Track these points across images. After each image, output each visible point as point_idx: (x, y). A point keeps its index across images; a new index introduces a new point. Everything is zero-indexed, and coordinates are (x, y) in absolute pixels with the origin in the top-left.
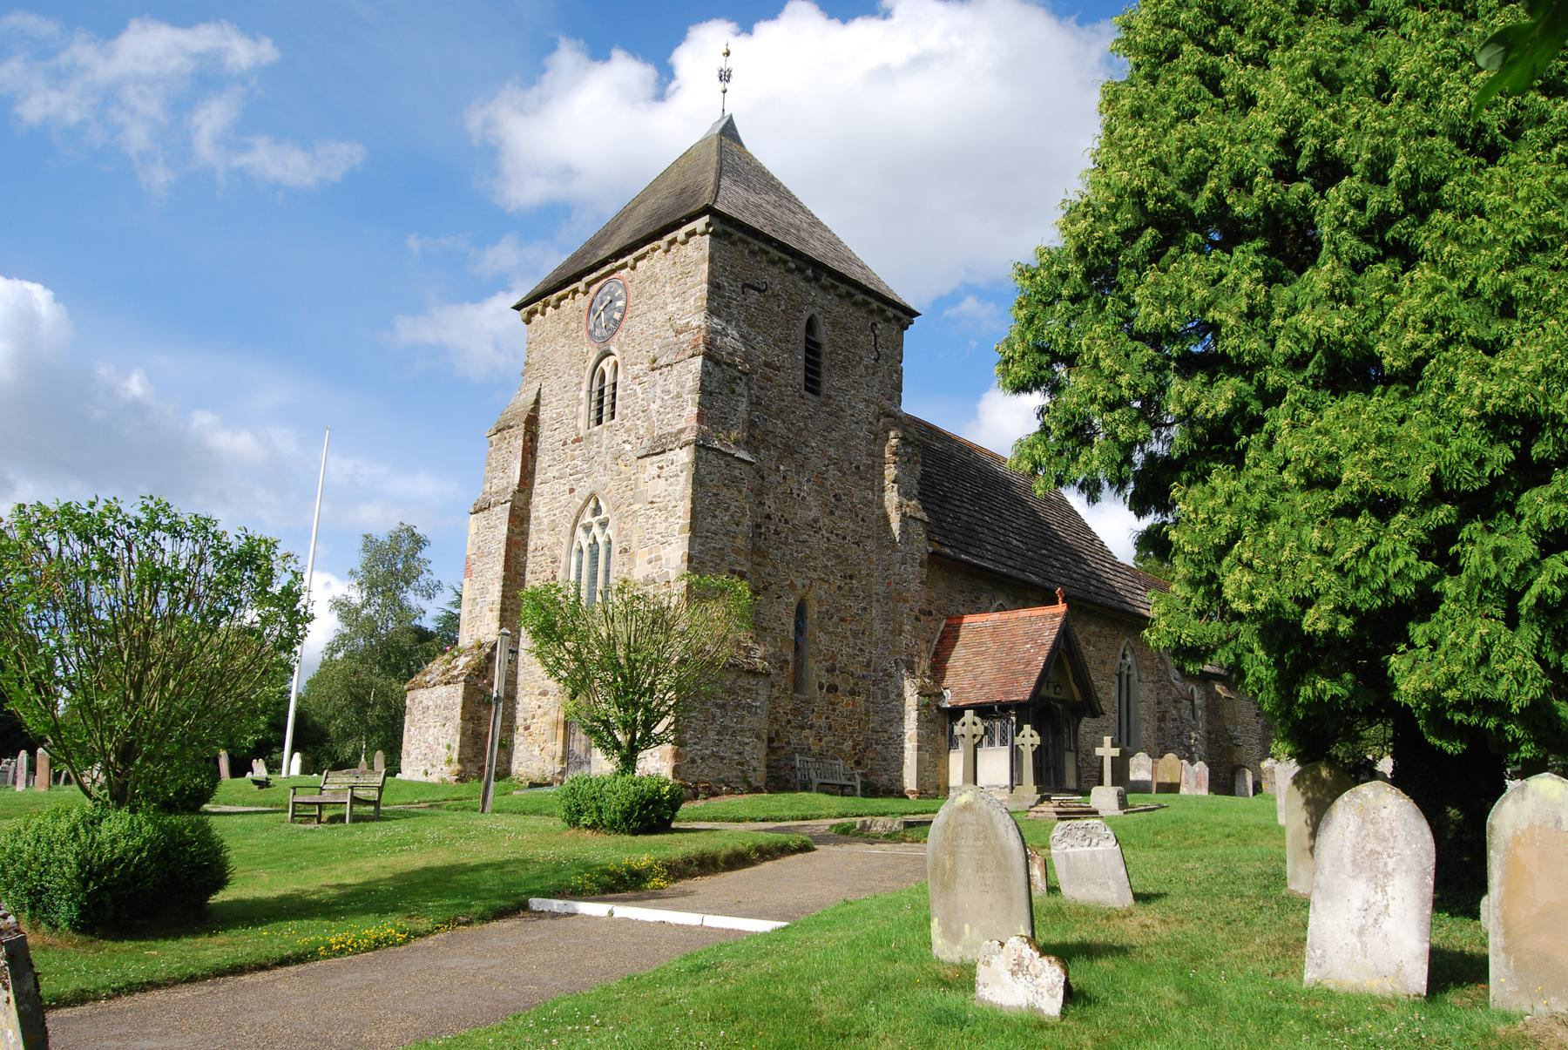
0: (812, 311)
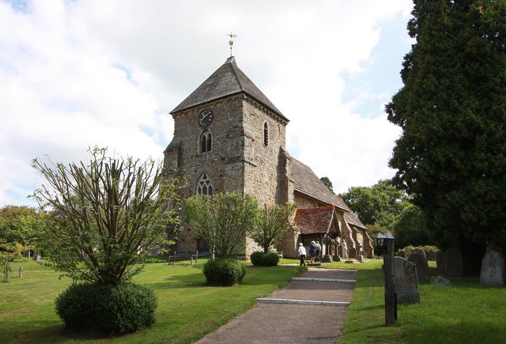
0: (266, 121)
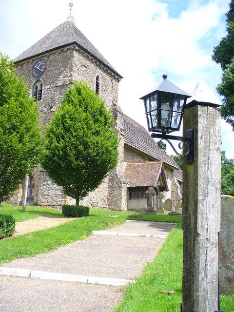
0: (98, 74)
